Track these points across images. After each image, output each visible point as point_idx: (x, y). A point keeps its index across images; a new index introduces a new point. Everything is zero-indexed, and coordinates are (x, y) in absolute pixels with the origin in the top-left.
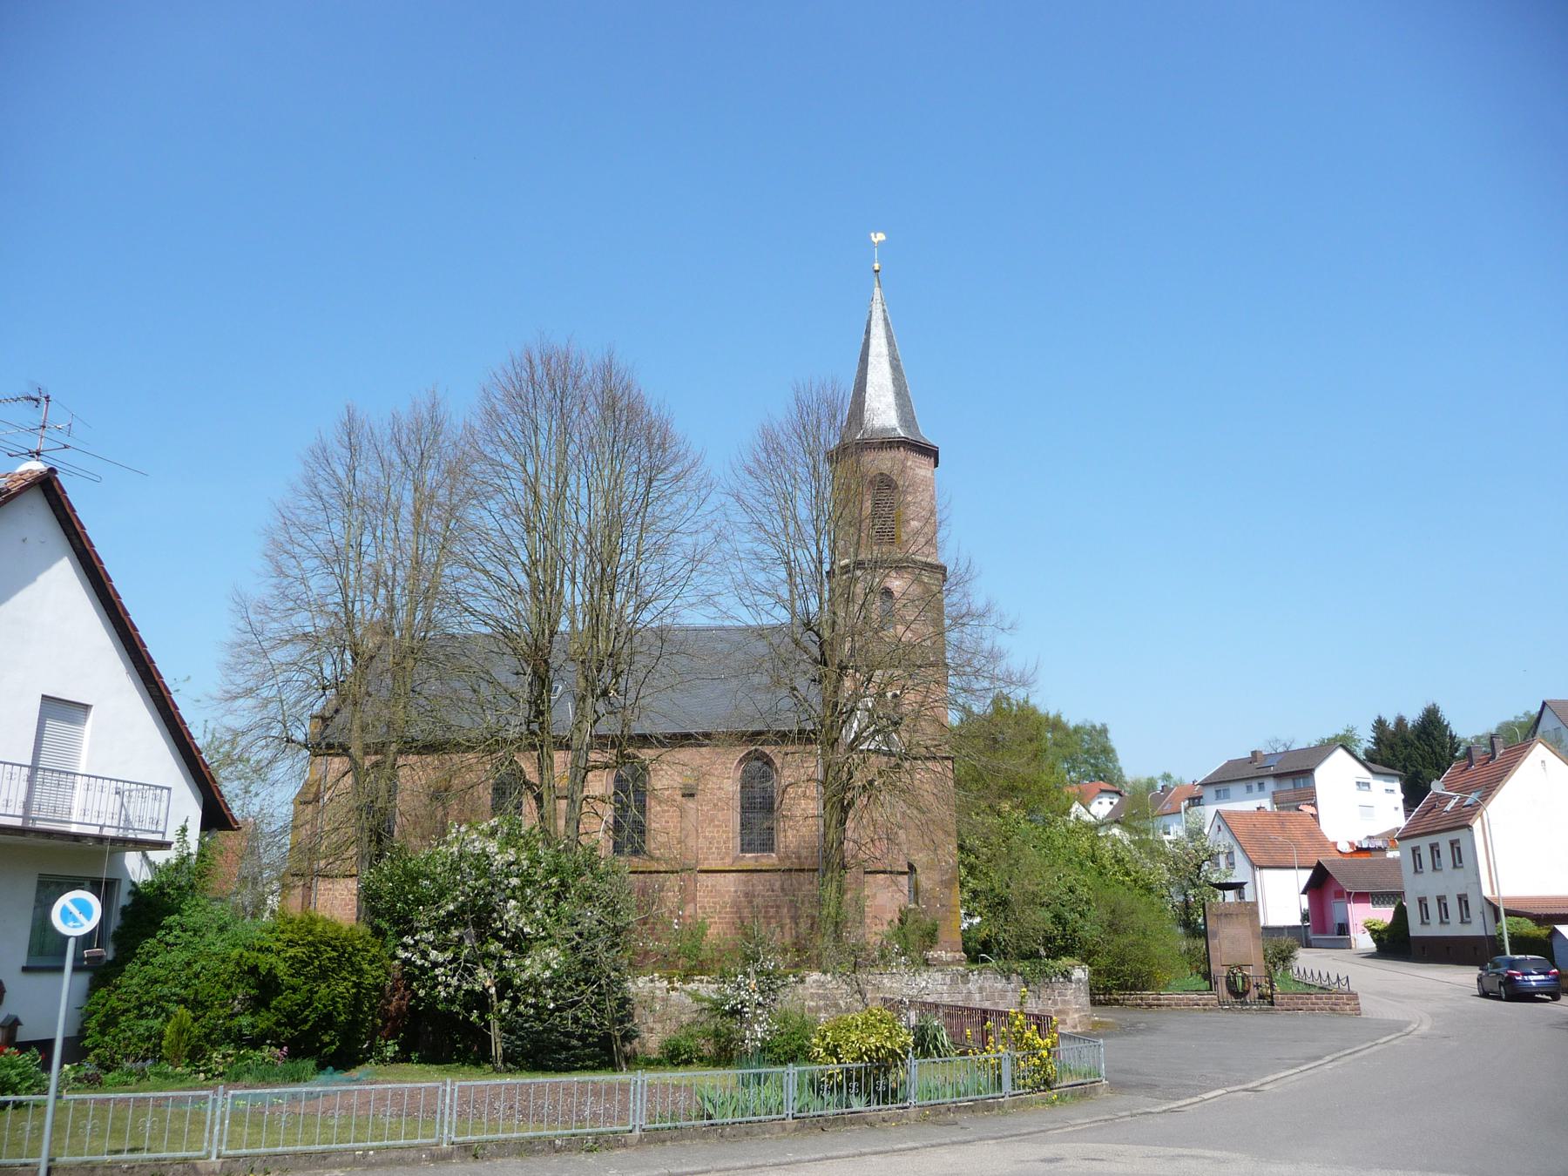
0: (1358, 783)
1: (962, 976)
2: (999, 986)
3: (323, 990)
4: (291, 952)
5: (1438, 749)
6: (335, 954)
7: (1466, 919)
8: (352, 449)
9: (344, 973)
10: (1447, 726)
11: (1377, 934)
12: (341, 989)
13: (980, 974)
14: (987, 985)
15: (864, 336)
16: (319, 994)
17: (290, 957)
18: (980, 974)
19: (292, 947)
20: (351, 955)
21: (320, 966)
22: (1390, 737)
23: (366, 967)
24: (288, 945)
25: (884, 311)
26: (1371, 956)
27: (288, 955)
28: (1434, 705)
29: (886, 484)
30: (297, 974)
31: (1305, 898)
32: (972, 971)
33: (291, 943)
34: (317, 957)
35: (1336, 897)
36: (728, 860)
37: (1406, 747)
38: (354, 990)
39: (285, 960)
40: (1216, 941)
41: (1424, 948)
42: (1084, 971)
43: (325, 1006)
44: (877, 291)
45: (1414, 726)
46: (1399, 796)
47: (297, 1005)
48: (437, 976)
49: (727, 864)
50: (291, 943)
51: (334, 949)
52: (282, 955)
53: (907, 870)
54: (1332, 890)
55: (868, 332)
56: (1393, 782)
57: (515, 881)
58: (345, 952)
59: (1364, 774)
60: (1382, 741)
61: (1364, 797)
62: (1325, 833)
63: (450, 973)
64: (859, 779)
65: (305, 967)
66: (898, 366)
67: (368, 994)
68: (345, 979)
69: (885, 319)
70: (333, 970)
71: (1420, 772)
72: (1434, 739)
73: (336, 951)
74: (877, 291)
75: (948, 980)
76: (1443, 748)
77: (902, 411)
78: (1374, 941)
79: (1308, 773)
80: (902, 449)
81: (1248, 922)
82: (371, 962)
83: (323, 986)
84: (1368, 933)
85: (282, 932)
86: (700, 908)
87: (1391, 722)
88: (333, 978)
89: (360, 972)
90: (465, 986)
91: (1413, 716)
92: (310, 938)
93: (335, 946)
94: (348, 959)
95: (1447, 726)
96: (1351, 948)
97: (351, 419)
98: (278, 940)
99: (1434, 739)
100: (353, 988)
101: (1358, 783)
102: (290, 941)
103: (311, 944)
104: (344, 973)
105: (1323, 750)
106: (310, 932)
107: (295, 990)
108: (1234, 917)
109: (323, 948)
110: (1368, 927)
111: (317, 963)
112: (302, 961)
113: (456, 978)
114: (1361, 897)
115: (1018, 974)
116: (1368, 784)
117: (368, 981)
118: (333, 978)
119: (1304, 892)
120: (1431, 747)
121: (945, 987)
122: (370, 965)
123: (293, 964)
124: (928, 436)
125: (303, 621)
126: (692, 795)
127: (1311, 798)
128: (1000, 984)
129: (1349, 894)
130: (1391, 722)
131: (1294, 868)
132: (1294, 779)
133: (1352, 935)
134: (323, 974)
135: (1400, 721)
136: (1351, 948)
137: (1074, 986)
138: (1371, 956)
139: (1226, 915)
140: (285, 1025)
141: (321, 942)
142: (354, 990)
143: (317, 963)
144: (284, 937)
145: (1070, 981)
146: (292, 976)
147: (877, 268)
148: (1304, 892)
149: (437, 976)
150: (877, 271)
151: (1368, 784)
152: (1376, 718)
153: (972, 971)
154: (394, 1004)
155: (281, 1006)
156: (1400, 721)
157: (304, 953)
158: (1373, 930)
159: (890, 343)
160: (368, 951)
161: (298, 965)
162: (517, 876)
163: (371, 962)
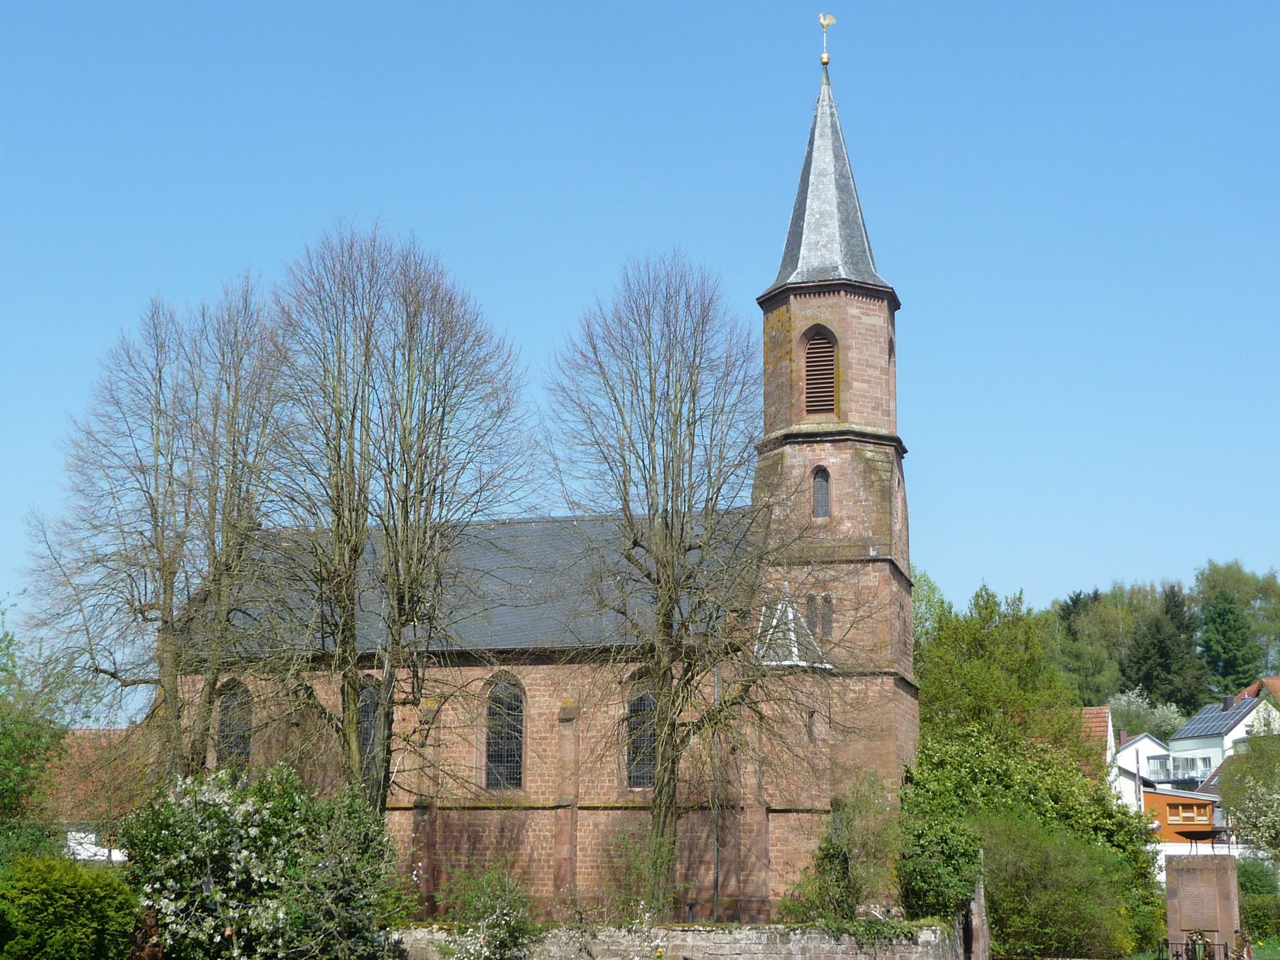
1: (781, 935)
2: (826, 947)
3: (59, 935)
4: (25, 899)
6: (71, 901)
8: (160, 347)
9: (82, 920)
12: (78, 935)
13: (803, 933)
14: (811, 945)
15: (806, 148)
16: (53, 939)
17: (24, 905)
18: (803, 933)
19: (27, 894)
20: (90, 902)
21: (54, 913)
23: (111, 913)
24: (22, 893)
25: (832, 115)
27: (21, 902)
29: (820, 336)
30: (32, 920)
32: (794, 930)
33: (25, 891)
34: (52, 905)
36: (614, 797)
38: (94, 936)
39: (19, 907)
40: (1176, 901)
42: (934, 932)
43: (57, 951)
44: (824, 88)
47: (27, 949)
48: (168, 924)
49: (612, 799)
50: (25, 891)
51: (70, 896)
52: (17, 902)
53: (829, 808)
55: (811, 143)
57: (254, 832)
58: (83, 899)
63: (180, 921)
65: (39, 913)
66: (847, 185)
67: (114, 940)
68: (84, 925)
69: (833, 125)
70: (71, 917)
73: (72, 898)
74: (824, 88)
75: (764, 938)
77: (848, 244)
80: (842, 293)
81: (1214, 879)
82: (118, 910)
83: (59, 931)
85: (19, 880)
86: (581, 850)
88: (70, 924)
89: (103, 919)
90: (192, 934)
92: (44, 886)
93: (71, 894)
94: (87, 906)
97: (155, 313)
98: (13, 887)
100: (92, 934)
102: (25, 889)
103: (44, 892)
104: (82, 920)
106: (45, 880)
107: (27, 935)
108: (1198, 872)
109: (57, 895)
111: (51, 910)
112: (36, 908)
113: (184, 927)
115: (850, 935)
117: (112, 927)
118: (70, 924)
121: (760, 947)
122: (117, 912)
123: (26, 911)
124: (885, 276)
125: (106, 544)
126: (570, 720)
128: (828, 945)
134: (59, 920)
137: (920, 949)
139: (1188, 870)
140: (1152, 944)
141: (56, 890)
142: (94, 936)
143: (51, 910)
144: (20, 885)
145: (916, 943)
146: (26, 922)
147: (825, 60)
149: (168, 924)
150: (826, 64)
153: (794, 930)
154: (147, 950)
155: (13, 950)
157: (37, 901)
159: (838, 156)
160: (114, 899)
161: (33, 912)
162: (258, 826)
163: (118, 910)
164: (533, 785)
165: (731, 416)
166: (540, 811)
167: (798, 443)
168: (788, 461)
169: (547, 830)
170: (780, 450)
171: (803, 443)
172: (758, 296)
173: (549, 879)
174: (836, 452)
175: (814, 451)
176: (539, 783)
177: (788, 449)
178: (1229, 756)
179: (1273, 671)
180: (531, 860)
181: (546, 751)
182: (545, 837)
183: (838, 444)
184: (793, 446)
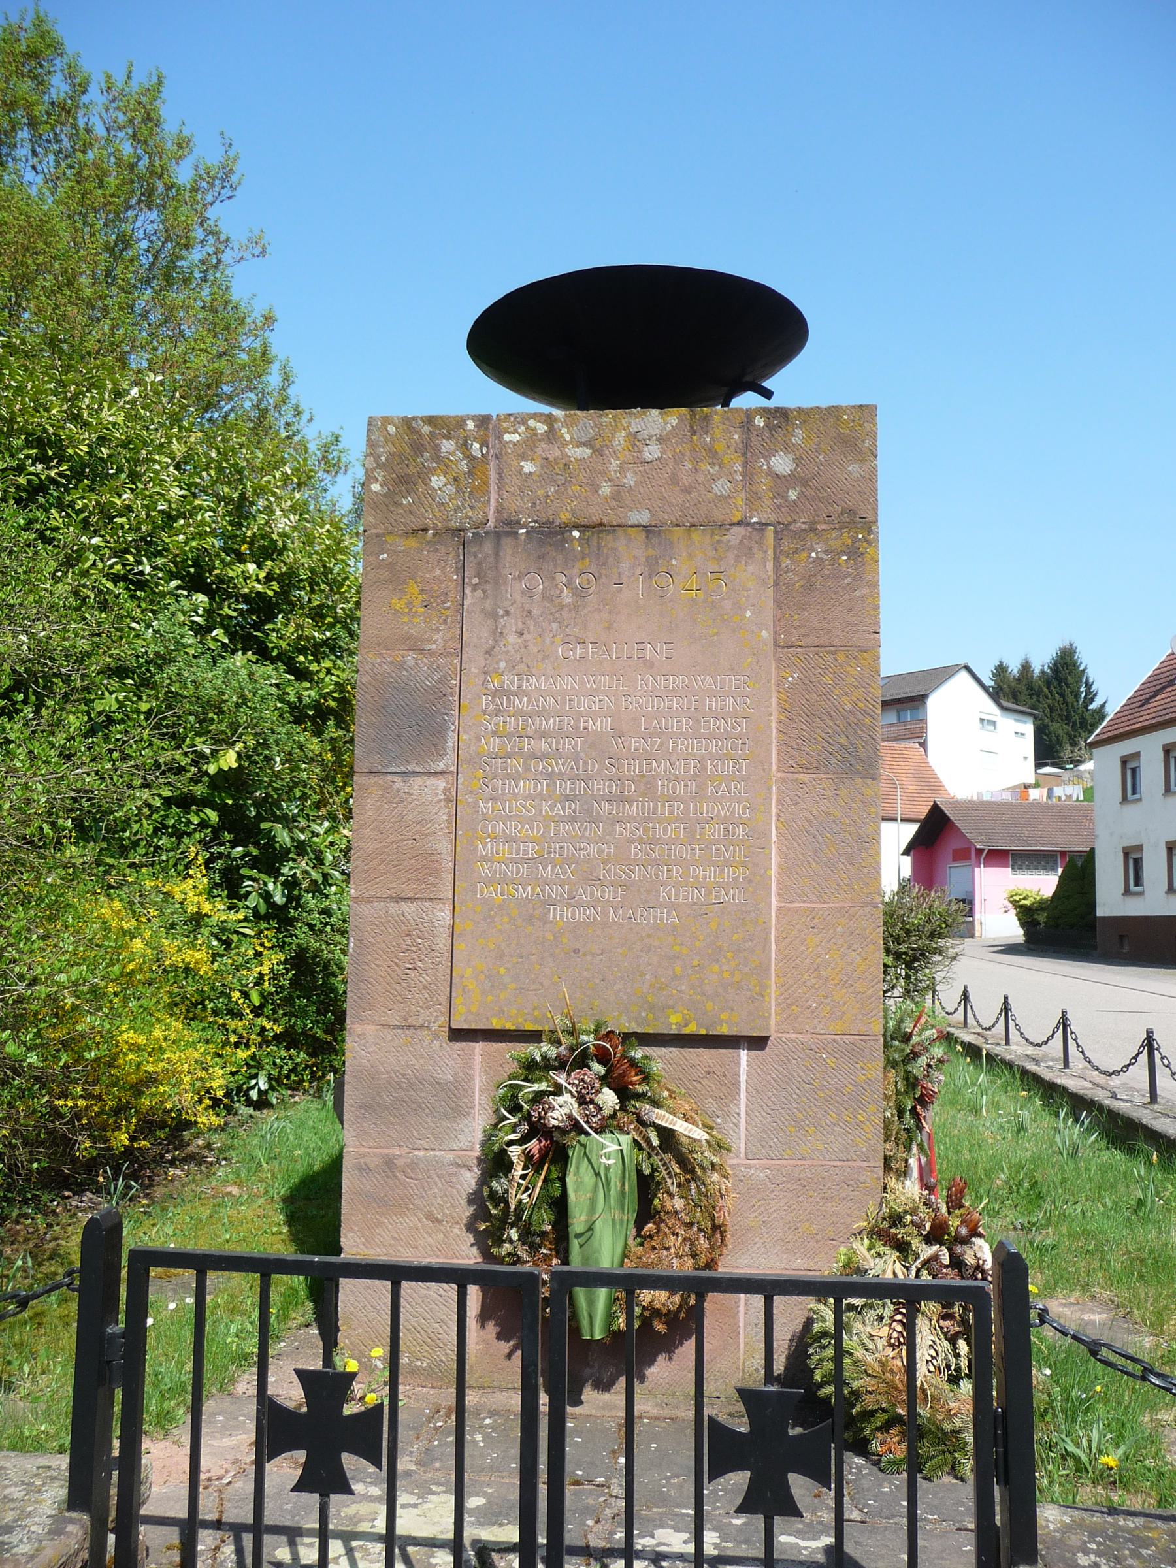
0: (982, 720)
5: (1070, 698)
7: (1132, 888)
10: (1083, 671)
11: (1027, 914)
22: (1013, 684)
26: (1011, 949)
28: (1071, 645)
31: (907, 861)
35: (955, 859)
37: (1031, 695)
41: (1121, 937)
45: (1043, 672)
46: (1027, 746)
54: (955, 844)
56: (1025, 722)
59: (989, 707)
60: (1001, 689)
61: (987, 738)
62: (939, 775)
64: (938, 979)
71: (1047, 726)
72: (1067, 685)
76: (1077, 696)
78: (1022, 925)
79: (917, 701)
84: (1013, 912)
87: (1014, 668)
91: (1042, 661)
95: (1083, 671)
96: (973, 936)
99: (1067, 685)
101: (982, 720)
105: (941, 675)
110: (1015, 903)
114: (997, 857)
116: (994, 723)
119: (906, 852)
120: (1062, 695)
127: (919, 735)
129: (979, 851)
130: (1014, 668)
131: (895, 820)
132: (898, 711)
133: (977, 916)
135: (1026, 667)
136: (973, 936)
138: (1011, 949)
148: (906, 852)
151: (994, 723)
152: (997, 663)
156: (1026, 667)
158: (1022, 907)
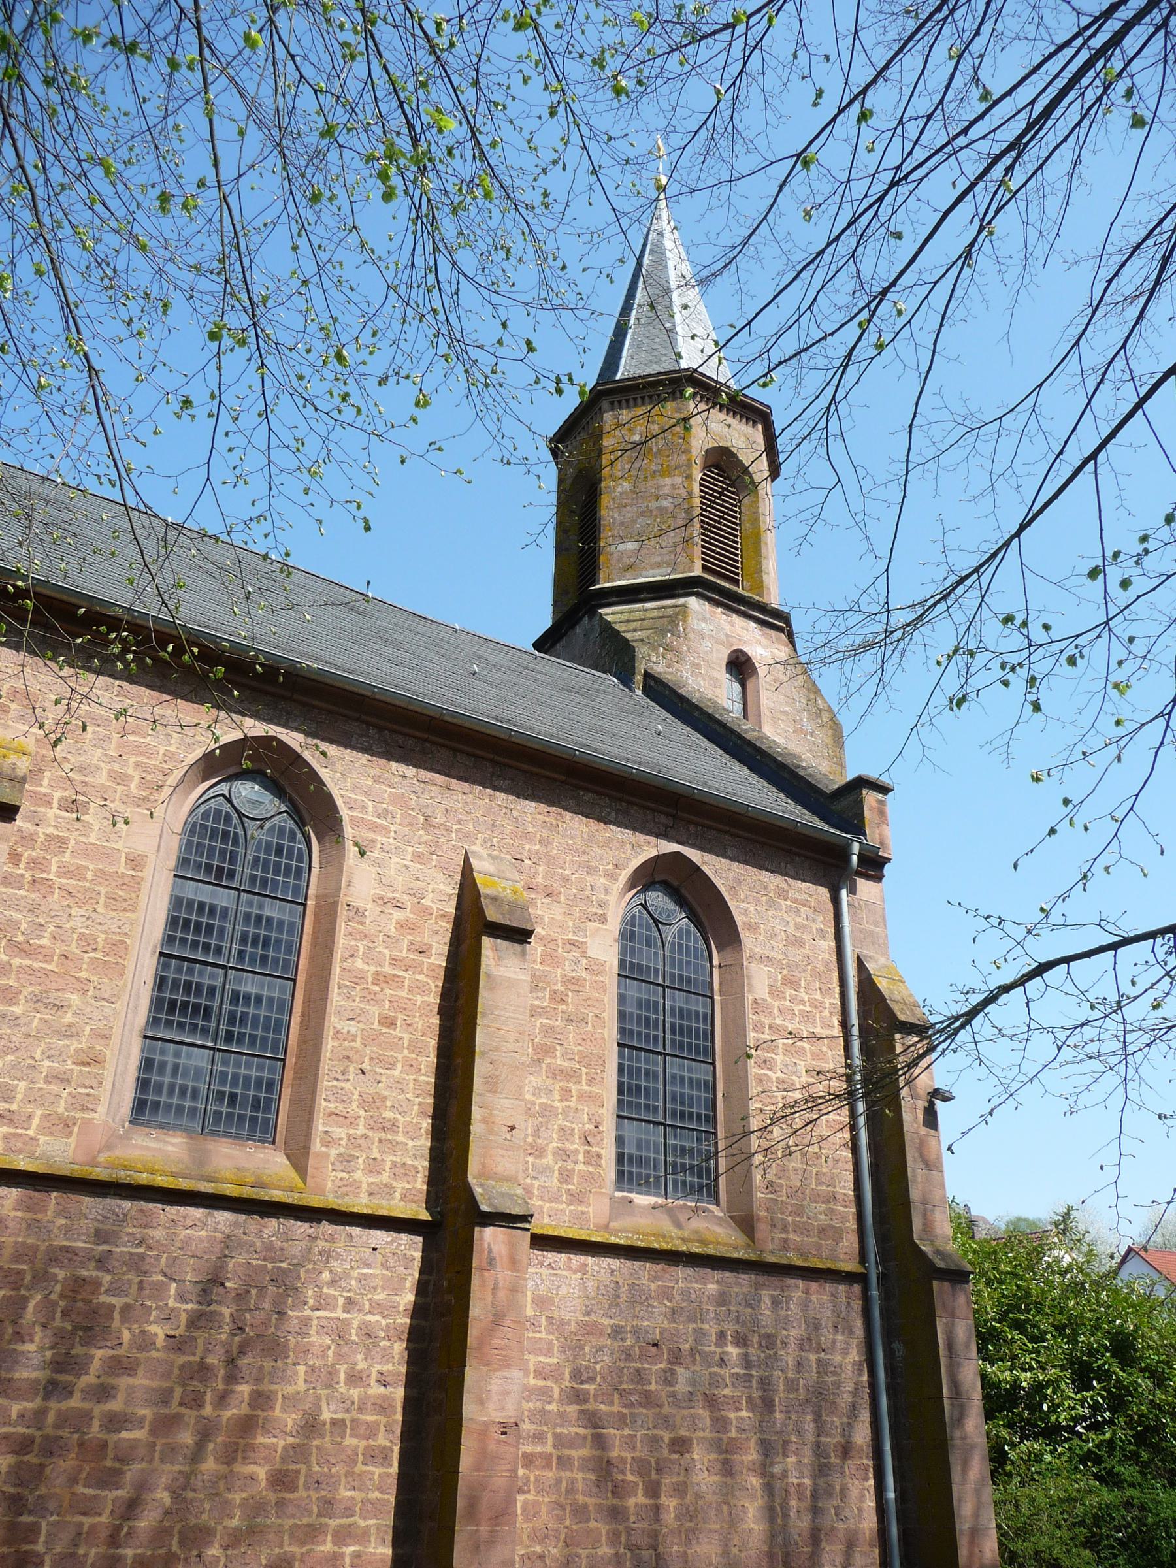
164: (340, 1132)
165: (637, 465)
166: (356, 1231)
167: (709, 600)
168: (694, 622)
169: (377, 1307)
170: (682, 601)
171: (718, 604)
172: (552, 428)
173: (370, 1508)
174: (764, 641)
175: (732, 624)
176: (361, 1130)
177: (693, 602)
178: (355, 1387)
179: (1064, 1264)
180: (311, 1426)
181: (392, 1024)
182: (368, 1333)
183: (767, 631)
184: (702, 602)
